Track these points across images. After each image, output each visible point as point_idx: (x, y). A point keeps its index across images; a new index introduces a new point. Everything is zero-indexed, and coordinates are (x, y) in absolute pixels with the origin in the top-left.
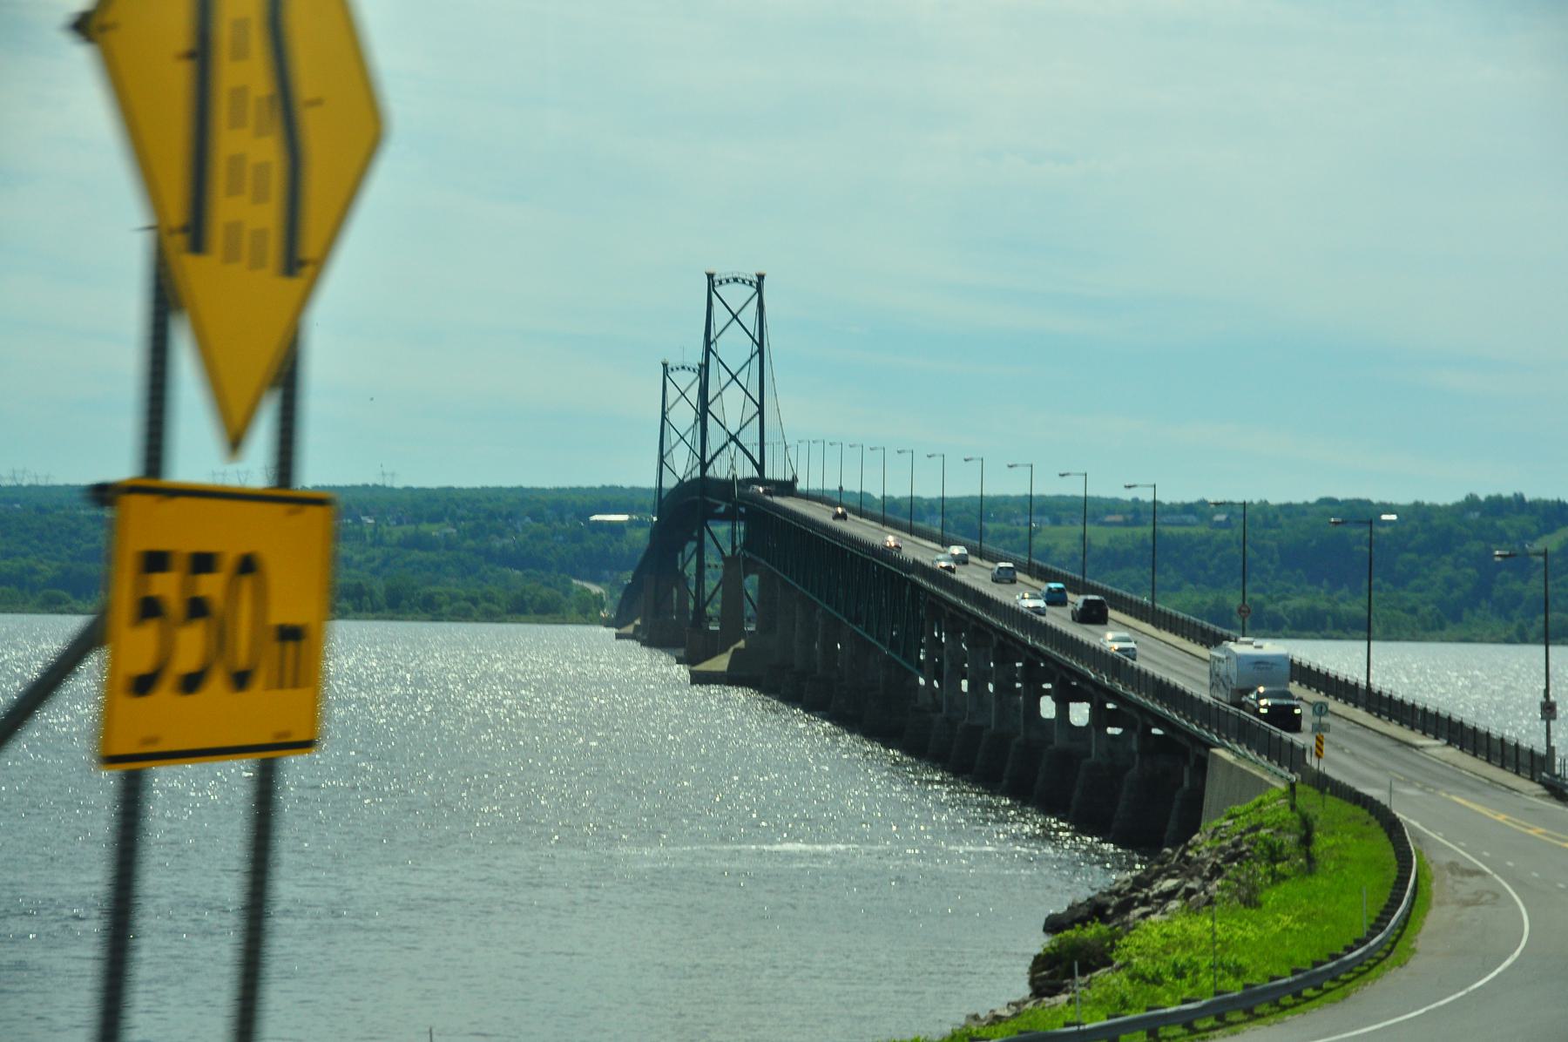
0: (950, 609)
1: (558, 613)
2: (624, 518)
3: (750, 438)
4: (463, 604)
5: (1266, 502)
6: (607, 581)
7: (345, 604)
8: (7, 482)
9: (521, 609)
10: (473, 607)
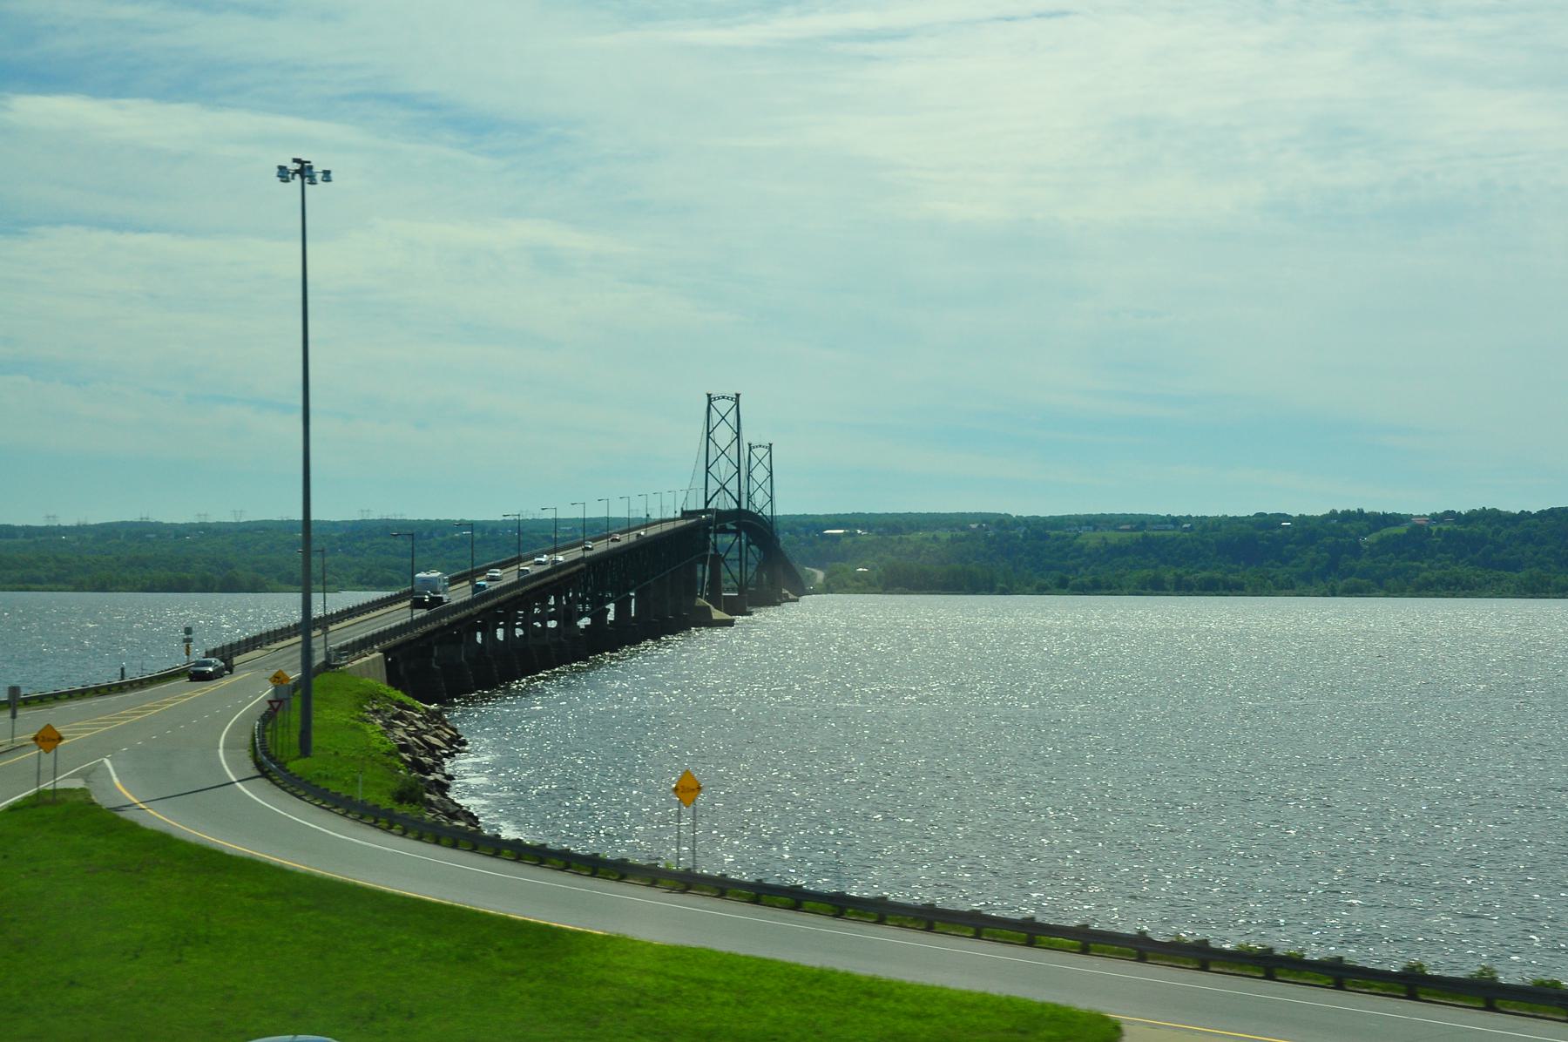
2: (842, 531)
3: (732, 486)
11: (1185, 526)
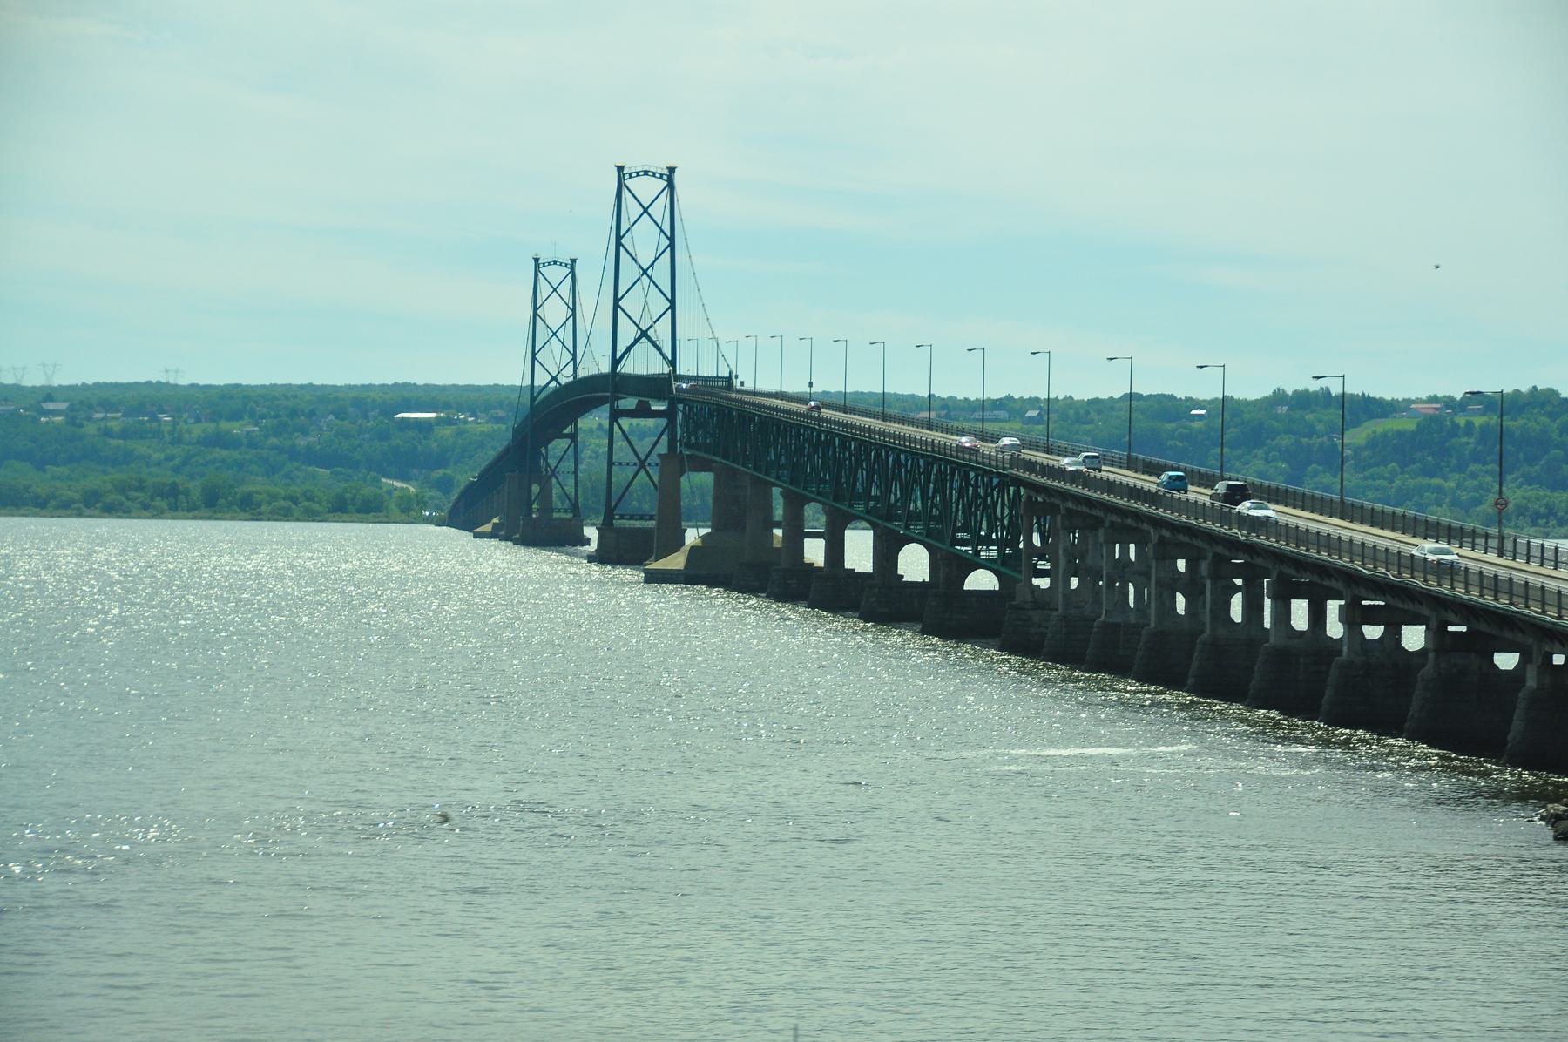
0: (1070, 505)
1: (381, 511)
2: (433, 415)
3: (662, 332)
4: (282, 503)
5: (1071, 397)
6: (416, 480)
7: (158, 502)
8: (9, 380)
9: (342, 508)
10: (294, 506)
11: (1030, 413)
